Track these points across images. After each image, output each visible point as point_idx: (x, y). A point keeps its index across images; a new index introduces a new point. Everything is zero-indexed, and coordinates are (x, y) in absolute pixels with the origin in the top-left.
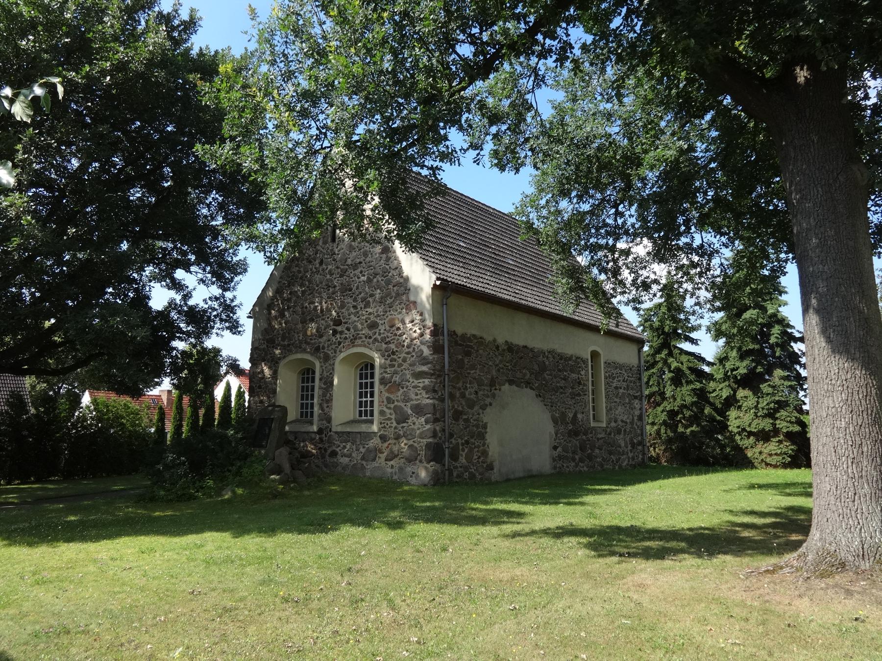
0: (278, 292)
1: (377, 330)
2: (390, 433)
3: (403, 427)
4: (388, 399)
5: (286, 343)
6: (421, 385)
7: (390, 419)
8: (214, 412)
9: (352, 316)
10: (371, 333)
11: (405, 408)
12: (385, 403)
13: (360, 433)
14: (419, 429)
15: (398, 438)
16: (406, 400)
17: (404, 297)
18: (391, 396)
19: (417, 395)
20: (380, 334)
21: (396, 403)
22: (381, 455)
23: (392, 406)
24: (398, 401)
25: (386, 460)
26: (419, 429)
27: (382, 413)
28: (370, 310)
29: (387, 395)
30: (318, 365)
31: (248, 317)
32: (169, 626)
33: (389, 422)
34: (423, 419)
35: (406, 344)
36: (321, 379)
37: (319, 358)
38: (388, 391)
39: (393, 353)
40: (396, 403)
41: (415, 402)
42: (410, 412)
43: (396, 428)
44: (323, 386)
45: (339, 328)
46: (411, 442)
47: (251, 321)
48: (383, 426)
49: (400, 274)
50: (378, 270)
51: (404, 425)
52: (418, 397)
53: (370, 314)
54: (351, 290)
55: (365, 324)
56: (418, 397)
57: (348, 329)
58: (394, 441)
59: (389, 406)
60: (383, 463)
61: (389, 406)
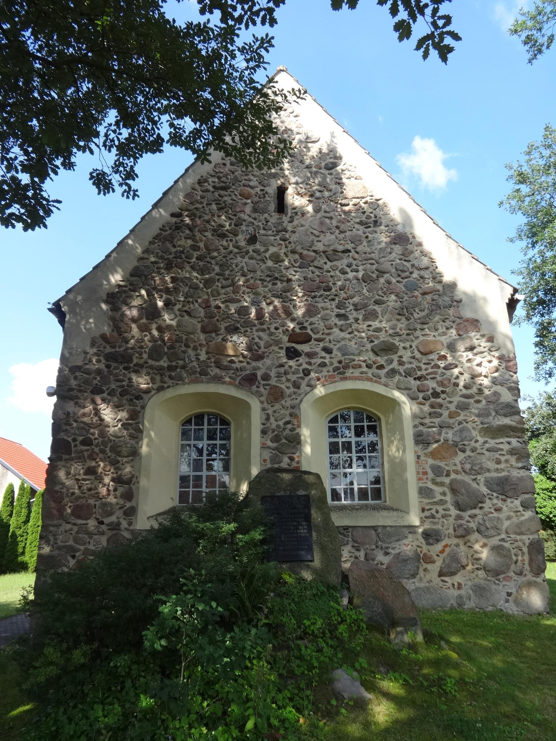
0: (138, 277)
1: (395, 358)
2: (447, 526)
3: (473, 517)
4: (437, 471)
5: (164, 363)
6: (506, 447)
7: (442, 502)
8: (15, 710)
9: (336, 330)
10: (381, 360)
11: (474, 485)
12: (431, 475)
13: (375, 528)
14: (509, 518)
15: (463, 534)
16: (476, 470)
17: (451, 311)
18: (442, 464)
19: (498, 462)
20: (401, 363)
21: (453, 476)
22: (429, 566)
23: (447, 480)
24: (457, 472)
25: (441, 574)
26: (509, 518)
27: (424, 492)
28: (376, 324)
29: (431, 461)
30: (255, 405)
31: (45, 226)
32: (255, 662)
33: (440, 508)
34: (517, 503)
35: (462, 384)
36: (264, 432)
37: (259, 394)
38: (433, 455)
39: (436, 395)
40: (453, 476)
41: (494, 475)
42: (484, 490)
43: (459, 517)
44: (269, 443)
45: (304, 348)
46: (495, 541)
47: (54, 399)
48: (427, 514)
49: (437, 277)
50: (387, 266)
51: (476, 511)
52: (502, 466)
53: (378, 330)
54: (329, 289)
55: (369, 346)
56: (502, 466)
57: (328, 351)
58: (455, 541)
59: (439, 480)
60: (437, 580)
61: (439, 480)
